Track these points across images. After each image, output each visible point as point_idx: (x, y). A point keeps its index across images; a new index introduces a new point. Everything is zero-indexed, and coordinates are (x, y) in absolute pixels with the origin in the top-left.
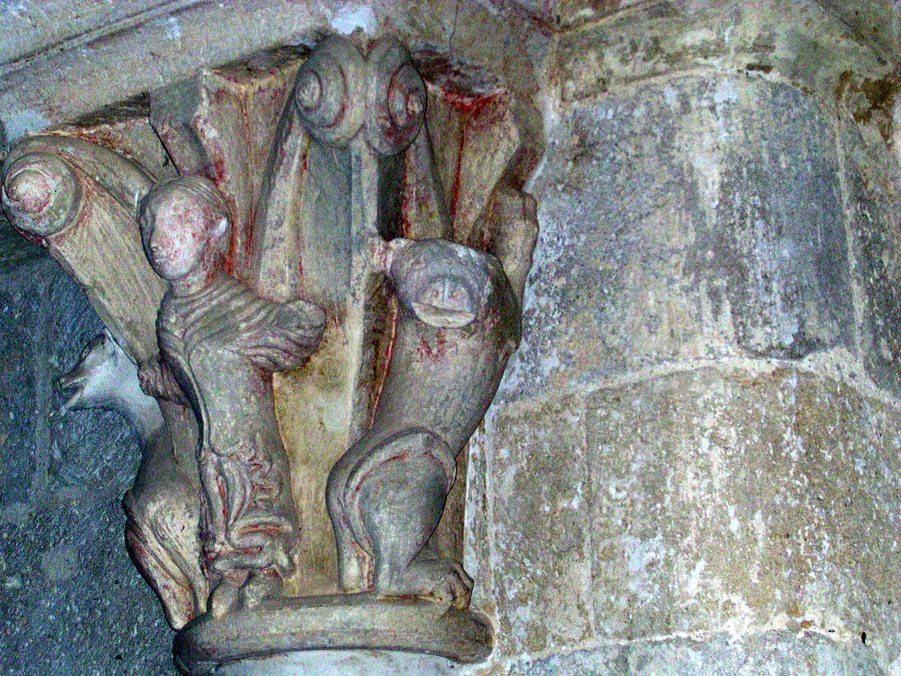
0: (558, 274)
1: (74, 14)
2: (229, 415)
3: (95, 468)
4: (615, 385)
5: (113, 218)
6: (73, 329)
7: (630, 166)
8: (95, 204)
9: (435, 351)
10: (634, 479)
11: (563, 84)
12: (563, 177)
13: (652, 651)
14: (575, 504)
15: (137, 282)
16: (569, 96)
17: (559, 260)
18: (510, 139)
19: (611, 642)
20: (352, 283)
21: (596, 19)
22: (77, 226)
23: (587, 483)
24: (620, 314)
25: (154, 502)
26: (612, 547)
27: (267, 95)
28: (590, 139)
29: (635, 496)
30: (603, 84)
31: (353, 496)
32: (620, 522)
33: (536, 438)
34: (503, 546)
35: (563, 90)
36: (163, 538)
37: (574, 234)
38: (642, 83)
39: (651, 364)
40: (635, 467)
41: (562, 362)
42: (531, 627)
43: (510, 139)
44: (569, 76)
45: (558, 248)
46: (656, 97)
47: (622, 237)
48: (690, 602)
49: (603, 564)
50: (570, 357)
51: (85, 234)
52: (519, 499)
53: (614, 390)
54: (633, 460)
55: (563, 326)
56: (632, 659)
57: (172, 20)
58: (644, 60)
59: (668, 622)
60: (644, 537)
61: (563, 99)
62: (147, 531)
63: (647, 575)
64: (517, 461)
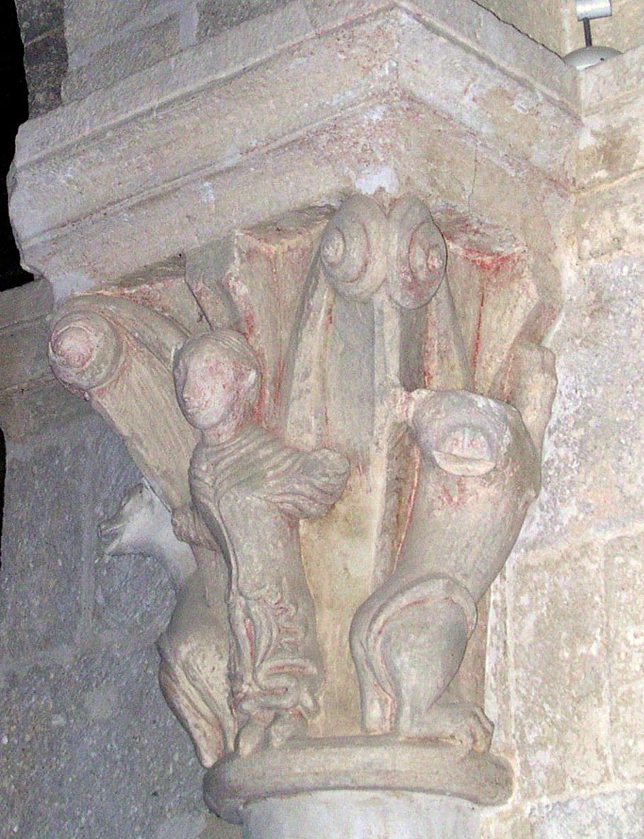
0: (577, 425)
5: (151, 373)
6: (118, 480)
9: (455, 499)
14: (594, 650)
15: (172, 433)
16: (586, 254)
21: (610, 180)
25: (186, 643)
28: (605, 296)
34: (523, 691)
36: (194, 679)
41: (580, 511)
44: (585, 235)
50: (589, 505)
57: (207, 184)
62: (179, 671)
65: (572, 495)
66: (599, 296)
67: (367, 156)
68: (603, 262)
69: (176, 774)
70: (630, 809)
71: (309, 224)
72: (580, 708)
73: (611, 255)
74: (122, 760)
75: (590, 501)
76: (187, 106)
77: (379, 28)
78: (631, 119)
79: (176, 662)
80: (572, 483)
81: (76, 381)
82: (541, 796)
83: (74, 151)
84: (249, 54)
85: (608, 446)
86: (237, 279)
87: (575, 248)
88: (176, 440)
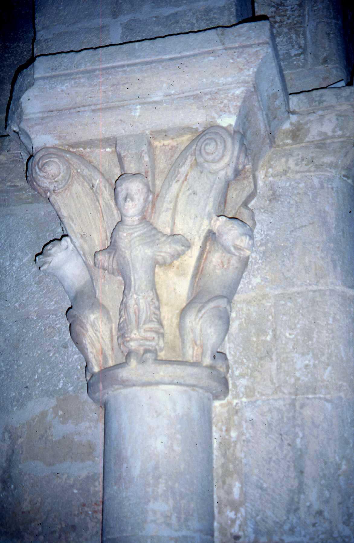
0: (261, 245)
1: (90, 96)
2: (143, 279)
3: (16, 302)
4: (289, 292)
5: (83, 189)
6: (5, 241)
7: (297, 206)
8: (75, 182)
9: (225, 266)
10: (298, 331)
11: (267, 169)
12: (264, 206)
13: (308, 401)
14: (269, 338)
15: (89, 219)
16: (269, 175)
17: (262, 239)
18: (250, 187)
19: (287, 396)
20: (200, 232)
21: (292, 145)
22: (66, 189)
23: (274, 331)
24: (292, 264)
25: (93, 314)
26: (287, 357)
27: (167, 148)
28: (277, 193)
29: (299, 337)
30: (285, 172)
31: (199, 320)
32: (291, 347)
33: (249, 310)
34: (232, 353)
35: (266, 172)
36: (97, 330)
37: (269, 229)
38: (303, 174)
39: (306, 285)
40: (298, 326)
42: (246, 387)
43: (250, 187)
44: (271, 167)
45: (261, 235)
46: (310, 181)
47: (293, 233)
48: (326, 383)
49: (283, 364)
50: (267, 279)
51: (69, 194)
52: (241, 334)
53: (289, 294)
54: (298, 323)
55: (263, 266)
56: (298, 404)
57: (138, 107)
58: (306, 165)
59: (315, 390)
60: (303, 354)
61: (266, 176)
62: (89, 327)
63: (304, 370)
64: (240, 319)
65: (259, 274)
66: (274, 194)
67: (226, 109)
68: (276, 179)
69: (39, 379)
70: (287, 406)
71: (181, 135)
72: (262, 362)
73: (281, 177)
74: (6, 371)
75: (268, 277)
76: (145, 68)
77: (257, 51)
78: (310, 120)
79: (87, 322)
80: (258, 269)
81: (48, 186)
82: (242, 398)
83: (74, 76)
84: (184, 50)
85: (277, 256)
86: (146, 153)
87: (264, 172)
88: (90, 222)
